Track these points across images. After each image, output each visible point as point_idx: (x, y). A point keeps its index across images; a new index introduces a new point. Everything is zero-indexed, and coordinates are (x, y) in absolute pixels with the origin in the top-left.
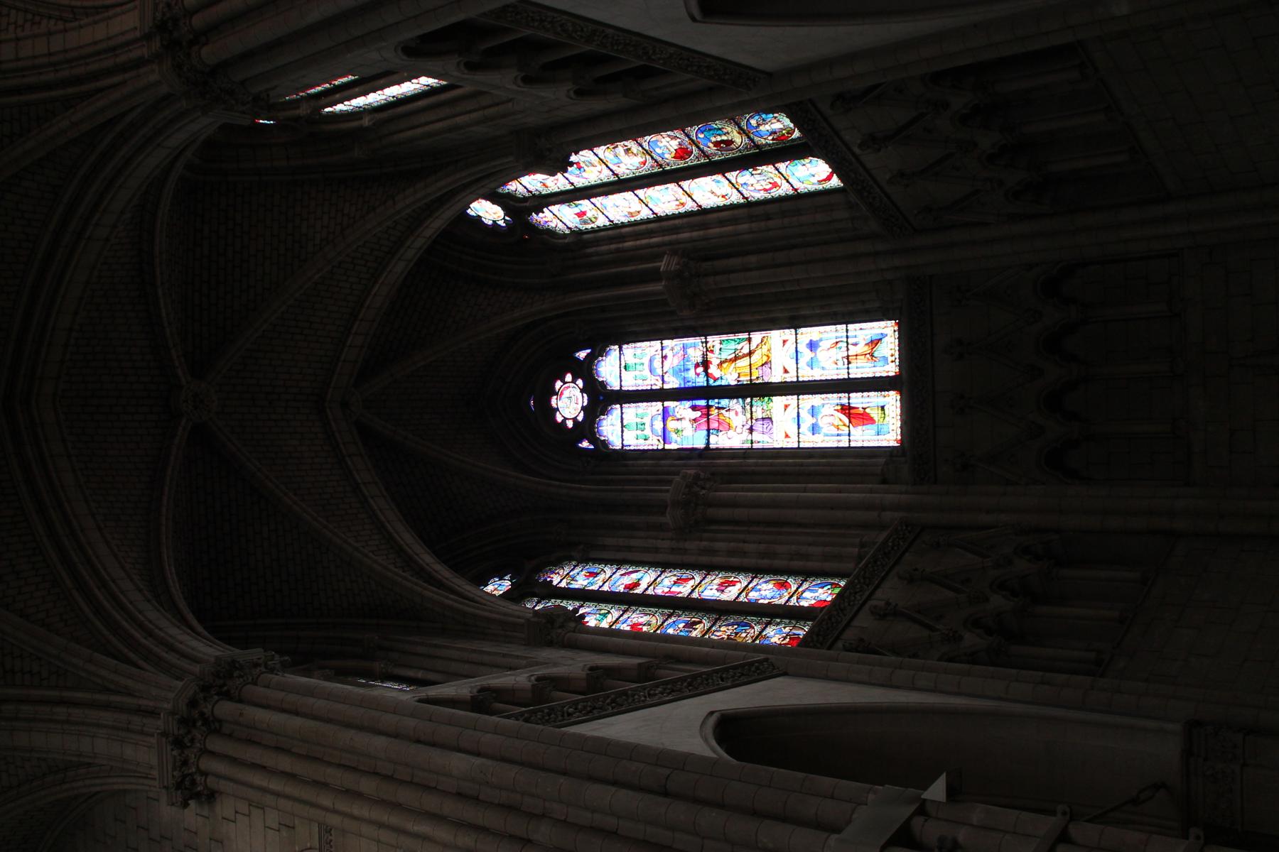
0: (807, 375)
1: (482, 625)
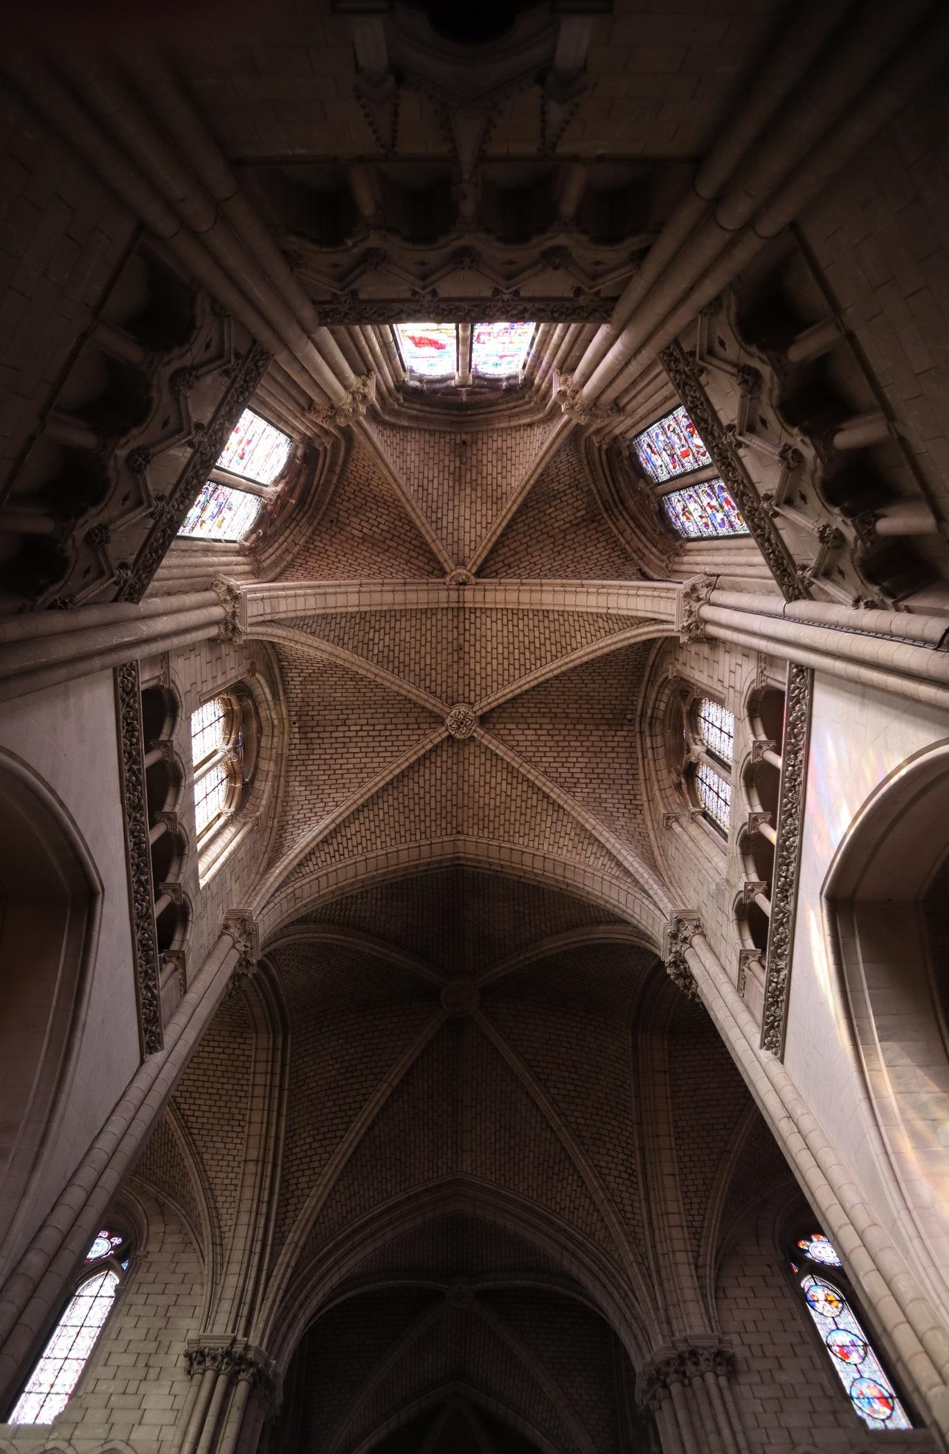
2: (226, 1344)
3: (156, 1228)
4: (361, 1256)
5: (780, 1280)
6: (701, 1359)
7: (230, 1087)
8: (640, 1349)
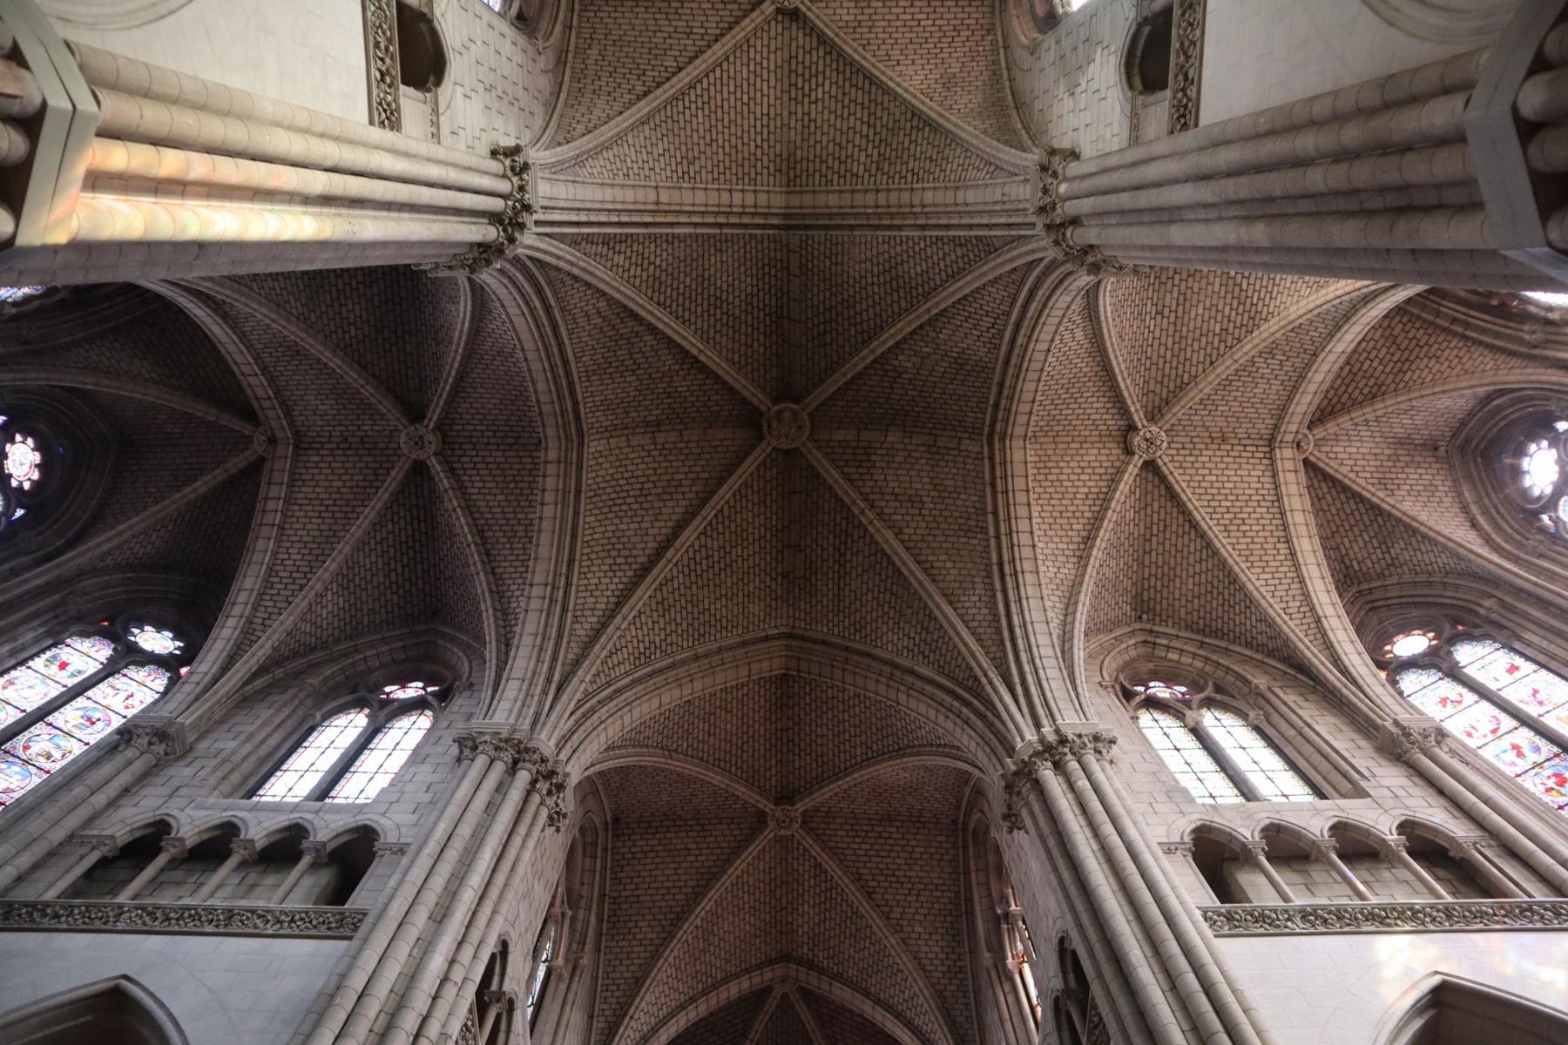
0: (80, 702)
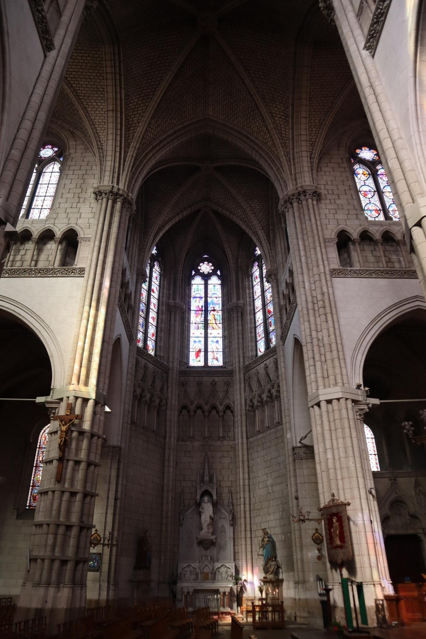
0: (210, 340)
1: (143, 249)
2: (110, 188)
3: (72, 143)
4: (164, 152)
5: (345, 165)
6: (307, 194)
7: (95, 74)
8: (282, 190)
